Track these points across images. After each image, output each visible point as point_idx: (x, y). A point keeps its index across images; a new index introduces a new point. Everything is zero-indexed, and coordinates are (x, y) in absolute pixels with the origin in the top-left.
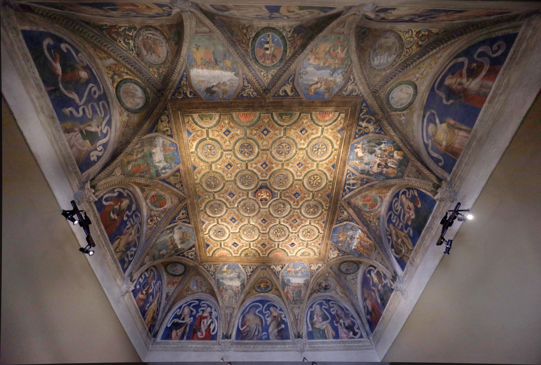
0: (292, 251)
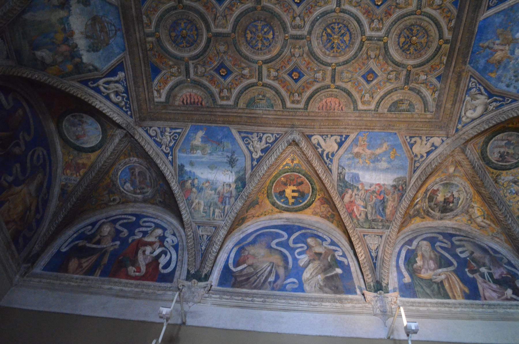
0: (367, 97)
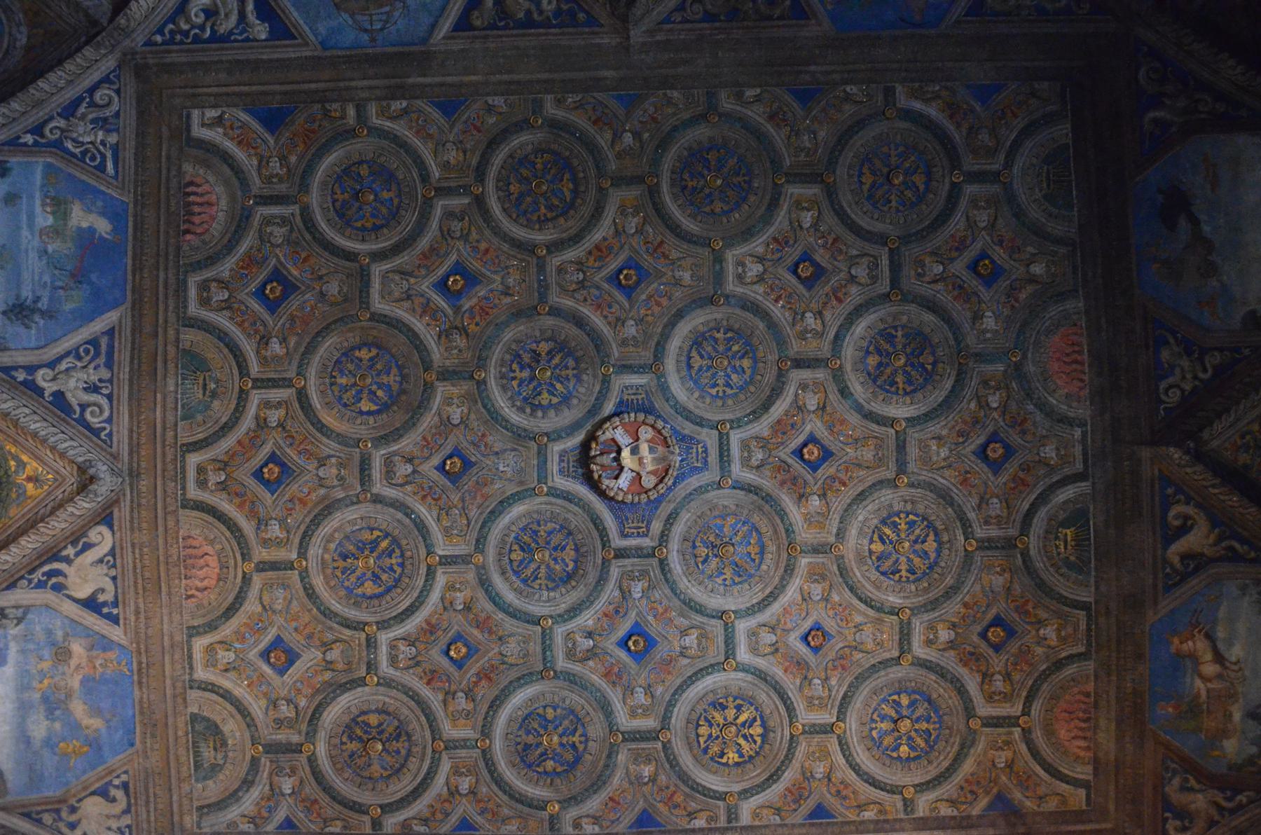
0: (225, 656)
